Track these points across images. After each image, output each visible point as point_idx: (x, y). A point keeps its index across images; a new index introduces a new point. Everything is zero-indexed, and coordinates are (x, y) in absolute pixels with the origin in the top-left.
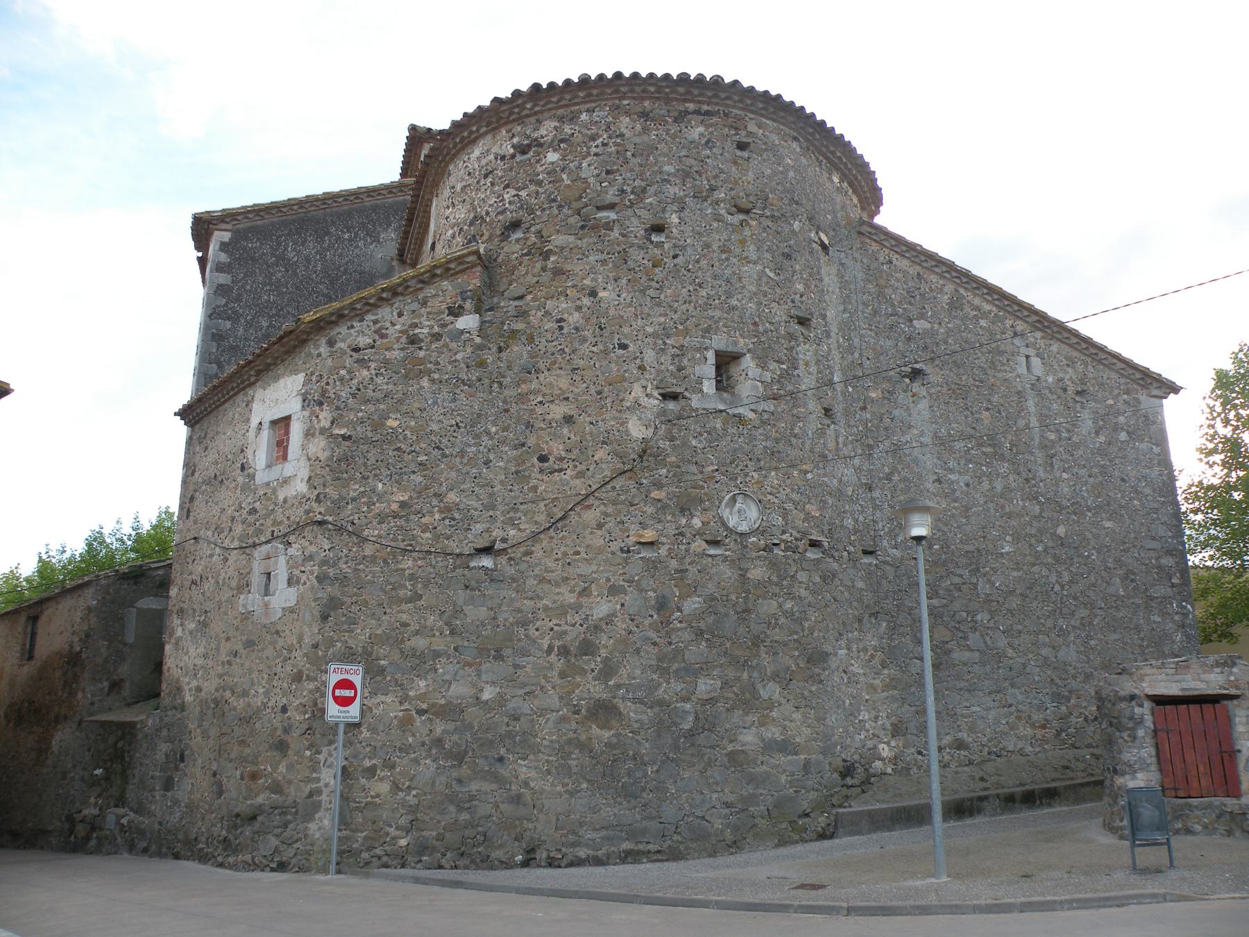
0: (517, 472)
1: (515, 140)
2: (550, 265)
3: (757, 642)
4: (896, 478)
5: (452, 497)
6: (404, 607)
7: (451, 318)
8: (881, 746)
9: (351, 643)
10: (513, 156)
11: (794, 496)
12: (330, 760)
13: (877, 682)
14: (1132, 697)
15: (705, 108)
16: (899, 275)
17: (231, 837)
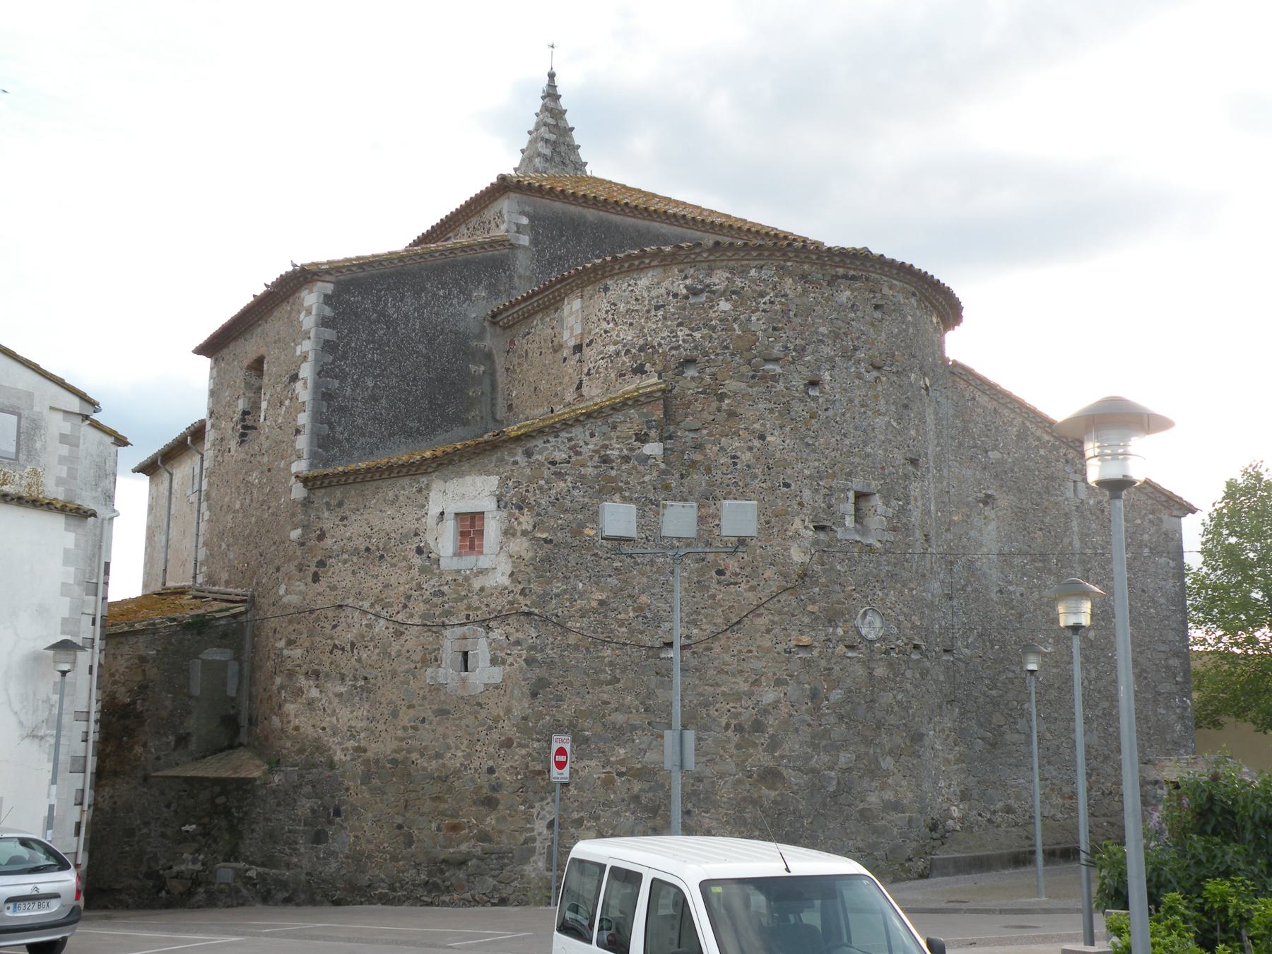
0: (698, 582)
1: (688, 282)
2: (725, 407)
3: (879, 725)
4: (969, 589)
5: (644, 599)
6: (605, 688)
7: (638, 444)
8: (953, 808)
9: (558, 716)
10: (686, 297)
11: (905, 609)
12: (543, 813)
13: (951, 757)
14: (1156, 782)
15: (852, 273)
16: (980, 411)
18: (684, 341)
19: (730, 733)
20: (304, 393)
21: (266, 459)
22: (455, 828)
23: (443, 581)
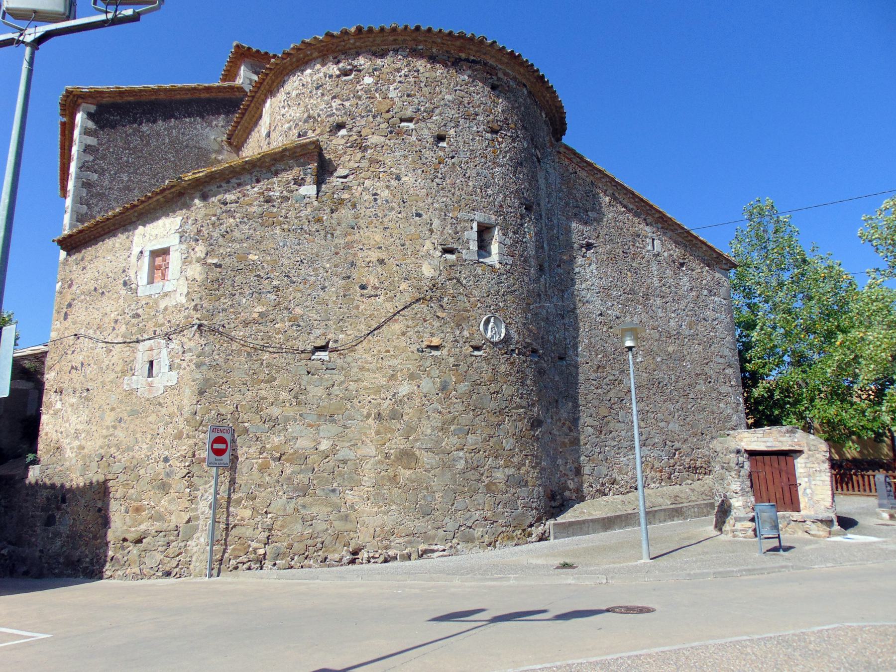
1: (341, 65)
5: (298, 311)
6: (264, 386)
7: (296, 187)
8: (569, 482)
9: (222, 411)
10: (338, 76)
13: (566, 440)
15: (472, 58)
16: (581, 181)
17: (119, 556)
18: (336, 109)
19: (370, 421)
22: (138, 510)
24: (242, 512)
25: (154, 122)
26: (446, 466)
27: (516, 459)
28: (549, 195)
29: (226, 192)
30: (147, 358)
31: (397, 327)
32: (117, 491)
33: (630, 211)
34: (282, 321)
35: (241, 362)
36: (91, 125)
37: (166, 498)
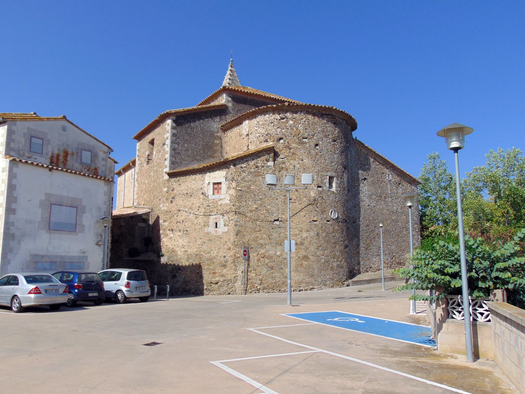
1: (281, 115)
5: (269, 207)
10: (280, 120)
20: (167, 148)
21: (155, 168)
23: (210, 202)
24: (252, 275)
25: (195, 122)
26: (319, 261)
27: (340, 259)
28: (351, 161)
29: (242, 163)
30: (215, 221)
31: (302, 214)
32: (205, 267)
33: (380, 164)
34: (263, 210)
35: (250, 225)
36: (174, 125)
37: (226, 269)
